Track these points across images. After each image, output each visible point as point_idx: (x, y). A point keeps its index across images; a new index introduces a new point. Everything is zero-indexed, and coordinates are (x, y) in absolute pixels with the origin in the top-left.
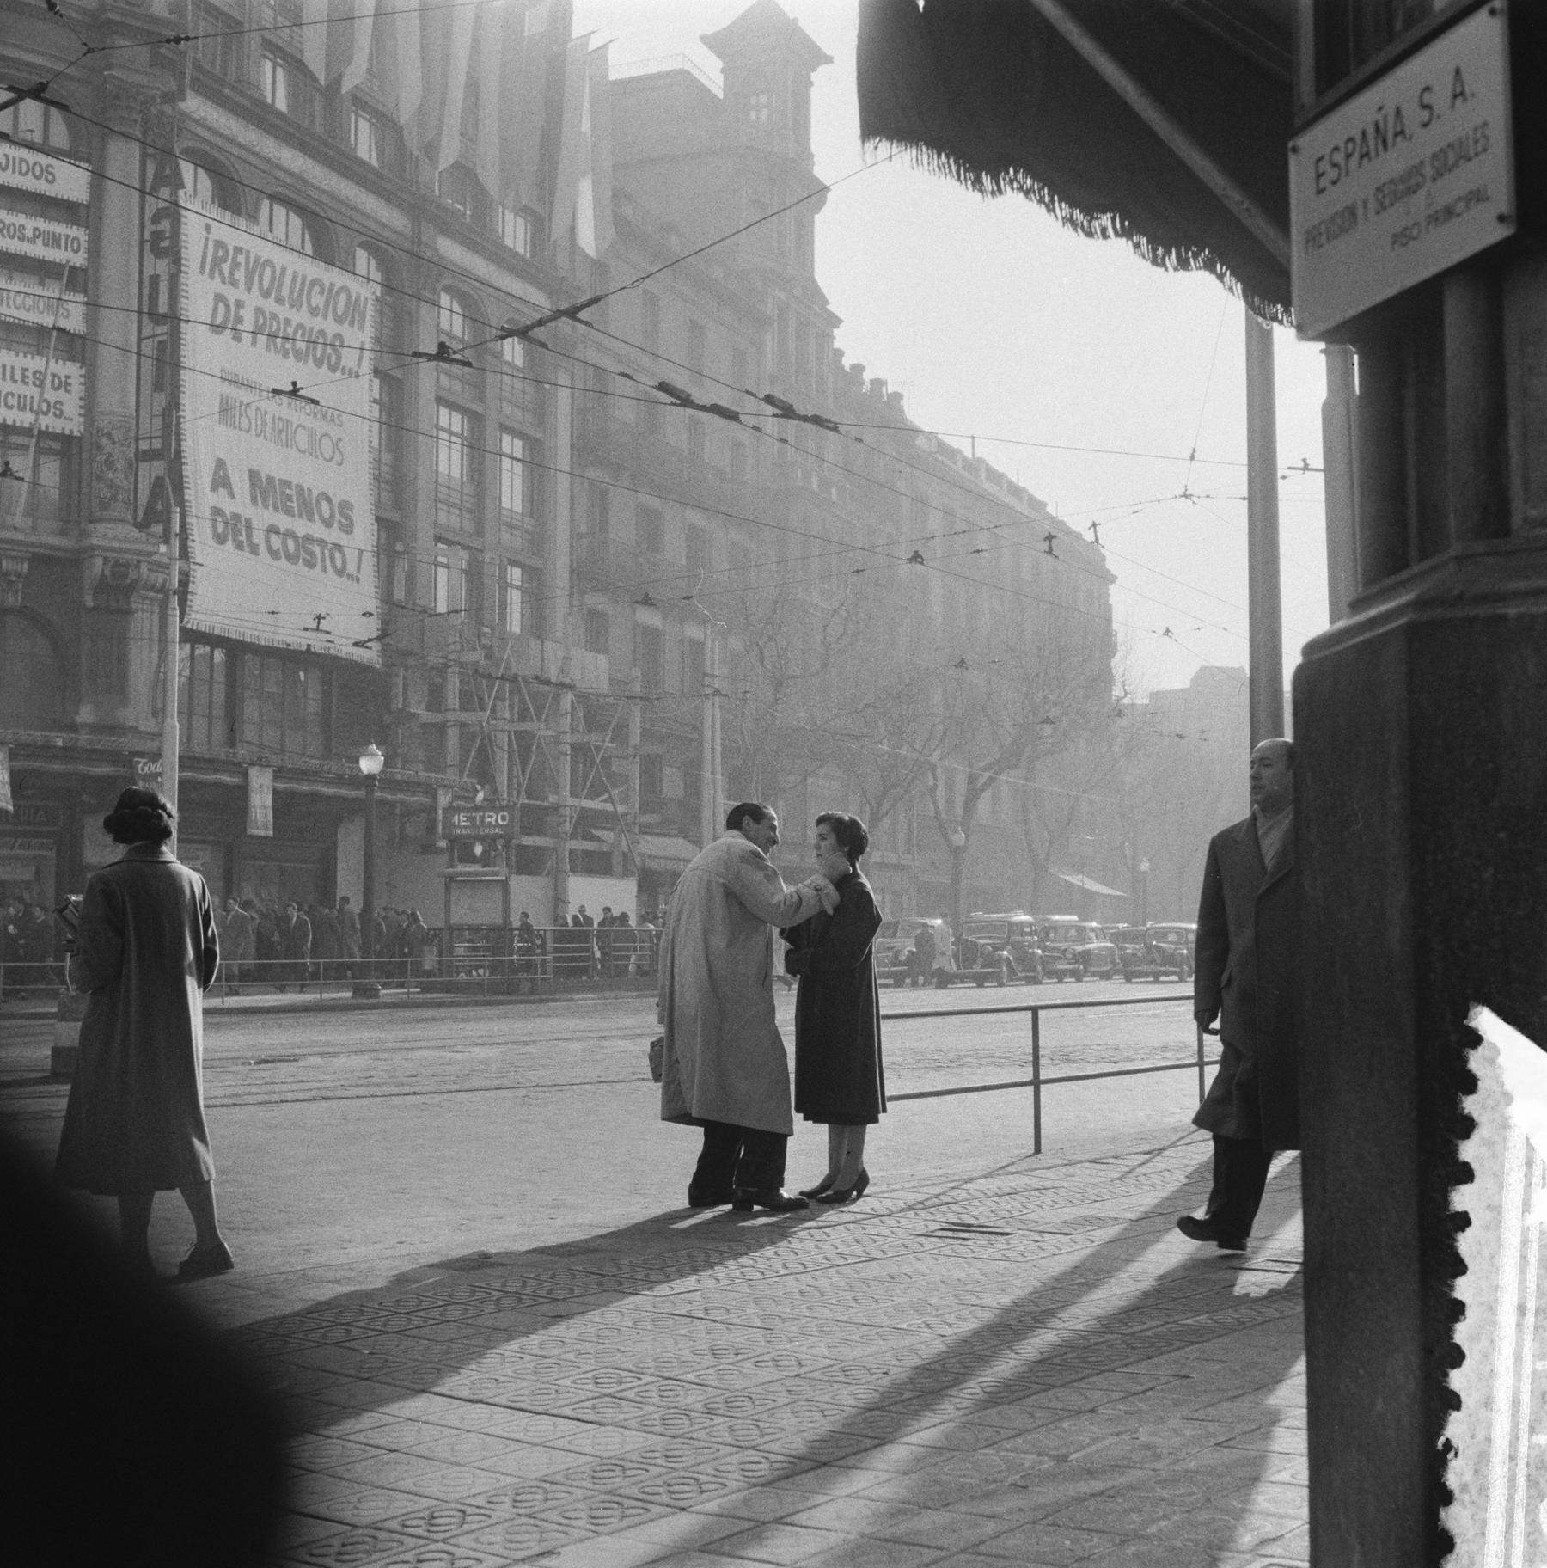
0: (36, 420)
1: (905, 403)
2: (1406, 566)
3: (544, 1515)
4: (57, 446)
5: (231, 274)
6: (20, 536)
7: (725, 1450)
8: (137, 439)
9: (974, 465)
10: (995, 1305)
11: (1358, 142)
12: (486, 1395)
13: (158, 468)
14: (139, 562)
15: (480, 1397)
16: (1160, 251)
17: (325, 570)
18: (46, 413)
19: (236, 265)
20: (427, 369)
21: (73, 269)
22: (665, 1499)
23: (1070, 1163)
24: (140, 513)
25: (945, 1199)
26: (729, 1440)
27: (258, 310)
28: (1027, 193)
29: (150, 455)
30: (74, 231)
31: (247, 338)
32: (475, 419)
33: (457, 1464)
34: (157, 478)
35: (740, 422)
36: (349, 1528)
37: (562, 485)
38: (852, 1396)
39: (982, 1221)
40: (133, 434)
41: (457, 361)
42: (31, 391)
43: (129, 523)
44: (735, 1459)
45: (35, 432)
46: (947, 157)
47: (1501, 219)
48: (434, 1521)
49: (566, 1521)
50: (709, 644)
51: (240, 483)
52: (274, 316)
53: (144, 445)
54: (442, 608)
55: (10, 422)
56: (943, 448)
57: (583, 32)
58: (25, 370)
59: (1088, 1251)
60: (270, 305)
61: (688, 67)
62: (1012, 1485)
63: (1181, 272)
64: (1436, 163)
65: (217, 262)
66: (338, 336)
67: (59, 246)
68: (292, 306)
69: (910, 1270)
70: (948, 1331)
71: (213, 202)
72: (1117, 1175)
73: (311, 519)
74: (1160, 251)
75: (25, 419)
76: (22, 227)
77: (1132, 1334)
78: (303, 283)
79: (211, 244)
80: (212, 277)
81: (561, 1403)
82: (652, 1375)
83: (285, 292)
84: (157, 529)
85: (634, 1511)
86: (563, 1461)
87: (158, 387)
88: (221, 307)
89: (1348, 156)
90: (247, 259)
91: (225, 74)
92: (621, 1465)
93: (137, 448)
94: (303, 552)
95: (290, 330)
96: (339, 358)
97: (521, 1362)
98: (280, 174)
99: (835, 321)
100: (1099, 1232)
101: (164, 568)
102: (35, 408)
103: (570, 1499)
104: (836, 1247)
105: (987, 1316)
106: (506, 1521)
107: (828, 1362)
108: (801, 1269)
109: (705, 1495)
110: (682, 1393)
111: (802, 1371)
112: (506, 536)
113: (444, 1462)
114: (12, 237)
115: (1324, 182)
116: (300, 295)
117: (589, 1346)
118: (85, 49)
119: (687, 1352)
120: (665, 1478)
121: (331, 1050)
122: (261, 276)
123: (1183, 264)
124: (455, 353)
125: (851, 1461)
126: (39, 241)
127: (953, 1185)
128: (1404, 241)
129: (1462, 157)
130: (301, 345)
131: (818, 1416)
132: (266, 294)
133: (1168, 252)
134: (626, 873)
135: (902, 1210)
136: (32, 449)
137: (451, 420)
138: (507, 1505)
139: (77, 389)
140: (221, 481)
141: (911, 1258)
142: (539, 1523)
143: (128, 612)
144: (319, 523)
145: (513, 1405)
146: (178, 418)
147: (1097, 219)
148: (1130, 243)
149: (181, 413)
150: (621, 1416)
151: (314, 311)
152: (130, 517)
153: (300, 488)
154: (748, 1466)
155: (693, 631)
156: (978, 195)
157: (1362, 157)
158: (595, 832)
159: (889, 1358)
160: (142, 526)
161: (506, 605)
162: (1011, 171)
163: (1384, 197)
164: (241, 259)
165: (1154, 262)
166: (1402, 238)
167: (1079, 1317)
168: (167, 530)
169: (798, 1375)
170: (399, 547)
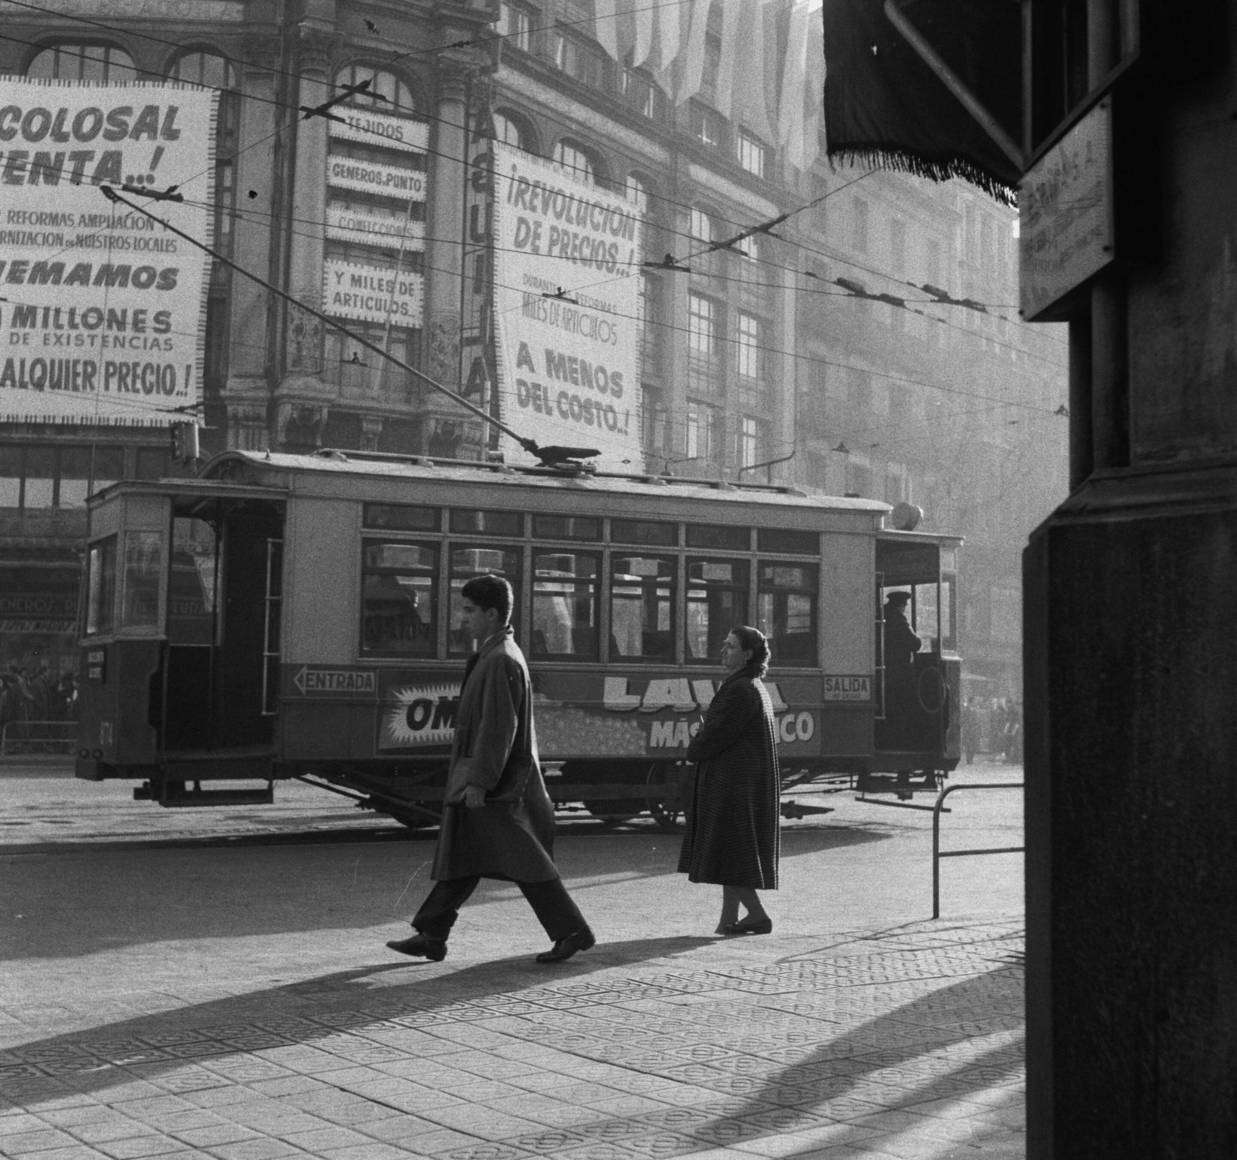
4: (403, 336)
5: (531, 201)
8: (462, 329)
12: (613, 1058)
13: (477, 350)
18: (395, 312)
24: (463, 388)
27: (554, 229)
29: (472, 341)
30: (417, 175)
32: (719, 306)
34: (476, 359)
42: (385, 296)
45: (387, 327)
46: (900, 156)
47: (1106, 249)
51: (539, 361)
52: (566, 233)
53: (467, 334)
58: (380, 280)
60: (562, 224)
65: (521, 193)
67: (405, 187)
68: (578, 224)
73: (591, 387)
75: (380, 317)
84: (476, 397)
86: (650, 1106)
87: (477, 290)
114: (371, 181)
124: (677, 262)
126: (391, 183)
132: (558, 216)
136: (385, 339)
137: (701, 307)
139: (418, 294)
140: (524, 359)
150: (705, 1079)
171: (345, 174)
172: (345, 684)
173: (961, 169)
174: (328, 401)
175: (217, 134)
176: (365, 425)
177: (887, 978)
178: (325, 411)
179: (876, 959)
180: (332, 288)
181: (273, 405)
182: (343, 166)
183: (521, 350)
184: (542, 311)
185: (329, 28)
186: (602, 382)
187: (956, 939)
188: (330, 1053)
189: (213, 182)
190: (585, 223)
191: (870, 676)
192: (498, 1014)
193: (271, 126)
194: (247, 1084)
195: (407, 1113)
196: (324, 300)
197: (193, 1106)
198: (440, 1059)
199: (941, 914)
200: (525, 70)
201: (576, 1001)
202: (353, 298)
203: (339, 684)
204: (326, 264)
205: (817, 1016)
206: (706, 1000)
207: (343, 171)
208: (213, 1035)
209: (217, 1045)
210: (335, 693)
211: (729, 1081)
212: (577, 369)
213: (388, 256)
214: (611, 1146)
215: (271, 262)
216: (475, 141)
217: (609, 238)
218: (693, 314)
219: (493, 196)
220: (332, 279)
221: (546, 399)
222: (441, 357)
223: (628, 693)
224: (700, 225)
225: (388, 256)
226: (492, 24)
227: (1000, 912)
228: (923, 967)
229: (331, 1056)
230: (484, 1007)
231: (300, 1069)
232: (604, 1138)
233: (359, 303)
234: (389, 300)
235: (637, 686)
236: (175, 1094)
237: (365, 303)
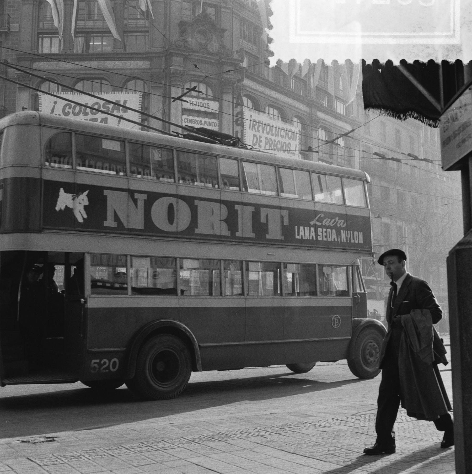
5: (258, 128)
12: (297, 452)
27: (266, 138)
36: (85, 456)
46: (389, 111)
50: (404, 227)
52: (271, 139)
60: (269, 136)
65: (254, 126)
76: (201, 121)
80: (252, 130)
82: (345, 449)
88: (255, 138)
91: (255, 73)
97: (309, 443)
98: (271, 99)
108: (402, 421)
116: (278, 133)
119: (357, 443)
122: (266, 128)
124: (313, 149)
126: (206, 124)
132: (268, 133)
134: (381, 299)
150: (333, 460)
151: (282, 137)
155: (399, 223)
156: (399, 121)
158: (371, 286)
162: (410, 112)
177: (403, 420)
182: (188, 119)
185: (182, 69)
190: (278, 136)
192: (254, 436)
193: (161, 106)
197: (142, 471)
200: (254, 80)
208: (149, 444)
209: (150, 448)
216: (236, 107)
217: (287, 141)
226: (241, 64)
231: (181, 457)
236: (135, 467)
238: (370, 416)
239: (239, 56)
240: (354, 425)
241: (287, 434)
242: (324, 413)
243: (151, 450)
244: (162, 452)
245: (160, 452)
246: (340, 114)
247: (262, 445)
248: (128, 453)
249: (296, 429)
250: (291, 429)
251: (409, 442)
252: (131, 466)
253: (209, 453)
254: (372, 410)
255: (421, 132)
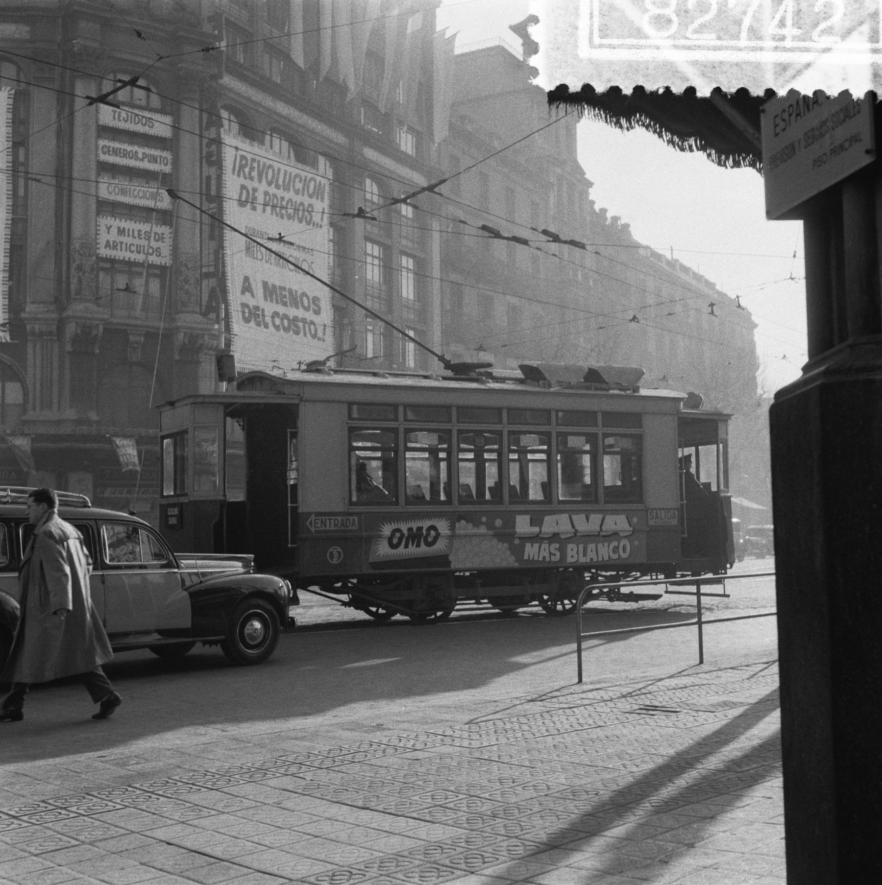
0: (146, 259)
1: (631, 229)
2: (832, 346)
3: (394, 875)
4: (157, 272)
5: (250, 173)
6: (139, 322)
7: (500, 838)
8: (201, 267)
9: (672, 264)
10: (665, 754)
11: (795, 106)
12: (372, 805)
13: (213, 282)
14: (203, 334)
15: (368, 806)
16: (723, 157)
17: (305, 335)
18: (152, 254)
19: (252, 169)
20: (359, 222)
21: (165, 174)
22: (463, 866)
23: (720, 669)
24: (203, 308)
25: (643, 691)
26: (503, 832)
27: (266, 193)
28: (647, 127)
29: (208, 275)
30: (165, 154)
31: (260, 208)
32: (387, 249)
33: (351, 845)
34: (212, 288)
35: (529, 245)
37: (436, 287)
38: (576, 809)
39: (664, 704)
40: (198, 264)
41: (369, 218)
42: (144, 242)
43: (196, 313)
44: (505, 844)
45: (146, 265)
46: (599, 110)
47: (868, 152)
48: (334, 878)
49: (406, 879)
51: (259, 291)
52: (275, 196)
53: (204, 270)
54: (370, 355)
55: (132, 260)
56: (654, 254)
57: (443, 28)
58: (139, 231)
59: (724, 722)
60: (272, 190)
61: (503, 44)
62: (660, 861)
63: (735, 169)
64: (834, 119)
65: (242, 167)
66: (310, 205)
67: (156, 162)
68: (284, 190)
69: (618, 733)
70: (635, 769)
71: (239, 134)
72: (745, 677)
73: (297, 307)
74: (723, 157)
75: (140, 258)
77: (742, 772)
78: (290, 176)
79: (238, 157)
81: (412, 810)
83: (280, 182)
84: (212, 316)
85: (444, 874)
86: (409, 844)
87: (212, 237)
88: (244, 192)
89: (790, 115)
90: (259, 167)
92: (440, 846)
93: (201, 272)
94: (293, 325)
95: (284, 203)
96: (311, 217)
99: (590, 184)
100: (731, 711)
101: (217, 337)
102: (146, 252)
103: (411, 865)
104: (578, 720)
105: (660, 761)
106: (374, 878)
107: (565, 787)
108: (556, 732)
109: (486, 865)
110: (480, 805)
111: (550, 792)
112: (405, 315)
113: (342, 843)
114: (131, 158)
115: (778, 130)
117: (430, 777)
118: (158, 57)
120: (465, 854)
121: (309, 604)
123: (737, 164)
124: (367, 213)
125: (571, 846)
126: (146, 160)
127: (650, 682)
128: (819, 163)
129: (847, 116)
130: (291, 211)
131: (554, 819)
132: (270, 184)
133: (727, 158)
135: (618, 698)
136: (145, 274)
137: (373, 250)
138: (375, 869)
139: (168, 241)
140: (247, 288)
141: (620, 726)
142: (392, 879)
143: (198, 362)
144: (301, 309)
145: (386, 811)
146: (223, 254)
147: (687, 140)
148: (705, 153)
149: (225, 252)
150: (445, 818)
152: (198, 309)
153: (290, 290)
154: (512, 848)
156: (618, 130)
157: (797, 115)
159: (599, 785)
160: (205, 315)
161: (405, 352)
162: (638, 115)
163: (809, 138)
164: (255, 165)
165: (719, 164)
166: (818, 162)
167: (714, 762)
168: (218, 317)
169: (546, 795)
170: (346, 321)
171: (111, 153)
172: (339, 525)
173: (642, 121)
174: (102, 320)
175: (13, 122)
176: (131, 337)
177: (558, 730)
178: (101, 328)
179: (546, 715)
180: (103, 238)
181: (61, 324)
182: (109, 147)
183: (244, 282)
184: (259, 253)
185: (96, 45)
186: (306, 304)
187: (599, 697)
188: (154, 814)
189: (10, 158)
190: (289, 189)
191: (676, 509)
192: (278, 775)
193: (54, 117)
194: (92, 844)
195: (223, 860)
196: (98, 246)
197: (52, 865)
198: (239, 814)
199: (584, 679)
200: (243, 78)
201: (334, 761)
202: (119, 245)
203: (336, 525)
204: (98, 219)
205: (516, 763)
206: (431, 755)
207: (109, 151)
208: (59, 804)
209: (63, 812)
210: (334, 531)
211: (464, 818)
212: (285, 295)
213: (145, 213)
214: (387, 878)
215: (56, 216)
216: (207, 128)
217: (307, 201)
218: (369, 255)
219: (222, 170)
220: (103, 229)
221: (264, 316)
222: (187, 287)
223: (531, 525)
224: (371, 191)
225: (145, 213)
226: (217, 43)
227: (624, 675)
228: (582, 721)
229: (154, 816)
230: (266, 770)
231: (133, 828)
232: (381, 872)
233: (124, 247)
234: (146, 245)
235: (536, 521)
236: (36, 855)
237: (129, 248)
238: (494, 724)
239: (214, 28)
240: (470, 744)
241: (344, 769)
242: (409, 722)
243: (66, 817)
244: (90, 820)
245: (86, 818)
246: (405, 153)
247: (296, 793)
248: (16, 826)
249: (359, 757)
250: (349, 757)
251: (582, 773)
252: (26, 854)
253: (192, 817)
254: (498, 712)
255: (552, 195)
